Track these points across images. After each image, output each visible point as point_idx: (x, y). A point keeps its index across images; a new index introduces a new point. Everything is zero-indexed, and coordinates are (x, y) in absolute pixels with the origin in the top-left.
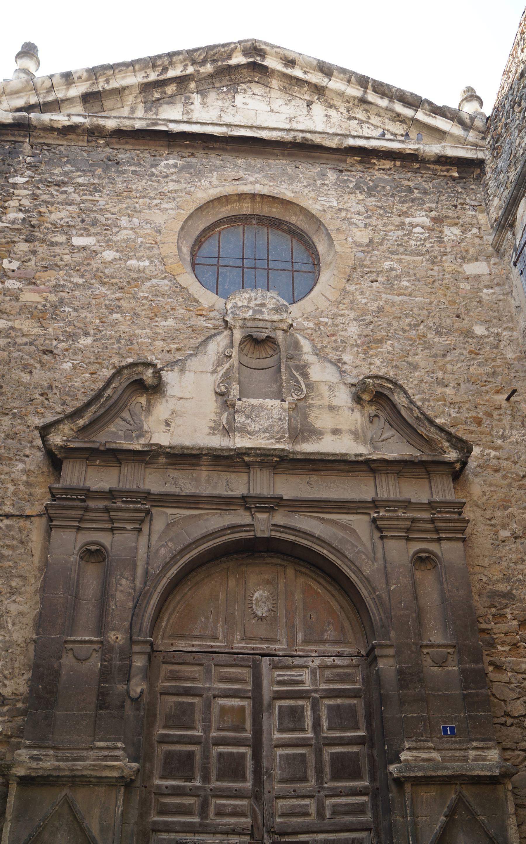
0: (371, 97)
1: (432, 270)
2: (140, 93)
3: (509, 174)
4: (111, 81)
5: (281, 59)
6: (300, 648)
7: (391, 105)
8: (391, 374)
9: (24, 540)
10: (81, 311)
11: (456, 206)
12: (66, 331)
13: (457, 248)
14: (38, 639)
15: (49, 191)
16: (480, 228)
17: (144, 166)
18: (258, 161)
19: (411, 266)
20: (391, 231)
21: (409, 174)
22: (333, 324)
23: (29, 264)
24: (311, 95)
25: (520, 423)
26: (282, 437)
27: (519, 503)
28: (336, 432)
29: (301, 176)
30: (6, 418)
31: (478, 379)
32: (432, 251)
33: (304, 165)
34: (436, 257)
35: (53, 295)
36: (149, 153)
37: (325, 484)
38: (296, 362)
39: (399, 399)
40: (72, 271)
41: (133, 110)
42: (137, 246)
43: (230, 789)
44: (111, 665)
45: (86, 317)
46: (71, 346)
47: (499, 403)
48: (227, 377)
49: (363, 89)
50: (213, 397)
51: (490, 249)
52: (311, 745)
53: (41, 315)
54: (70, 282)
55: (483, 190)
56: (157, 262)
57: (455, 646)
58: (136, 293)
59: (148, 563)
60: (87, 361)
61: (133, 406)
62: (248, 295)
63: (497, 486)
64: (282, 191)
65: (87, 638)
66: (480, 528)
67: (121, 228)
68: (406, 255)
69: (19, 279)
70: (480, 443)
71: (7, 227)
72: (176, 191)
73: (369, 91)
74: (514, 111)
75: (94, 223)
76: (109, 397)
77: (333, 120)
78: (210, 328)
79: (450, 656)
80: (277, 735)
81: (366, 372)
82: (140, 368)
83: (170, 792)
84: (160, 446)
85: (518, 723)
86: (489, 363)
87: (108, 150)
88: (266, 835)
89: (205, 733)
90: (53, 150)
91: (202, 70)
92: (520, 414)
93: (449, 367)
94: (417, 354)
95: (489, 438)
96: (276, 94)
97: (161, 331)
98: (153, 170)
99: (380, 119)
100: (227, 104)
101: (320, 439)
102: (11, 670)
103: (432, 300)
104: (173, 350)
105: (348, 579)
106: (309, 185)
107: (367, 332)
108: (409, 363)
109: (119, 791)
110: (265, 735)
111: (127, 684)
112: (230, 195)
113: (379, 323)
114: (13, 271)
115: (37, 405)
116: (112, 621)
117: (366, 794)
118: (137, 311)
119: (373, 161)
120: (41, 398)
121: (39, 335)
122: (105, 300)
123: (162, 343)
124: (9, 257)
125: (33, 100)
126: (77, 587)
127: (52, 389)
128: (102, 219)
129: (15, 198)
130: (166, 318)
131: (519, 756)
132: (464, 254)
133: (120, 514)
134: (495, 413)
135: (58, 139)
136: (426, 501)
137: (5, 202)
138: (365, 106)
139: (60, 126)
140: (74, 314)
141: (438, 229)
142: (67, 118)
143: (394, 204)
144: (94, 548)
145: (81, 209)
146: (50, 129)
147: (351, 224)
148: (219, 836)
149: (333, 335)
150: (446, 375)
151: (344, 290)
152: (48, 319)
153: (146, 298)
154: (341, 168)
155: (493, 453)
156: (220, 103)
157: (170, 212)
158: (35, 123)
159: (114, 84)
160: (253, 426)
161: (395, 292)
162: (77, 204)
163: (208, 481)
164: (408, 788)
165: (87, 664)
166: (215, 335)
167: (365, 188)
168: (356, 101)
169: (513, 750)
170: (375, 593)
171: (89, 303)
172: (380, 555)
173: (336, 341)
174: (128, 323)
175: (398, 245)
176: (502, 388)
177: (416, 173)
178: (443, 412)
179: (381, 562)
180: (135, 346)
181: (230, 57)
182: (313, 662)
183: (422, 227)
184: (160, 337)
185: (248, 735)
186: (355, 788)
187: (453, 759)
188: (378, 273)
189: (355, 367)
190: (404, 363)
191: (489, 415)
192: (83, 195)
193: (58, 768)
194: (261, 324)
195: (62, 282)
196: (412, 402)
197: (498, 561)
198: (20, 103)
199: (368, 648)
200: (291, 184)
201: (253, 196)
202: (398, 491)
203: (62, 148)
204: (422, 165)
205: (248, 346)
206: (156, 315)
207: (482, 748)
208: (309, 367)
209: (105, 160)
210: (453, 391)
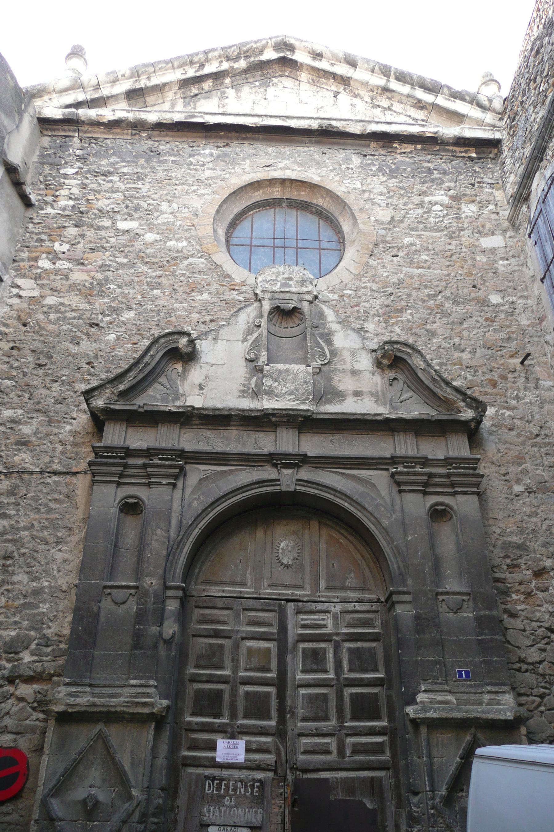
0: (394, 85)
1: (450, 244)
2: (179, 89)
3: (524, 150)
4: (152, 78)
5: (309, 52)
6: (323, 594)
7: (413, 92)
8: (410, 341)
9: (69, 495)
10: (124, 288)
11: (473, 185)
12: (111, 306)
13: (474, 224)
14: (79, 584)
15: (97, 180)
16: (496, 204)
17: (183, 156)
18: (287, 148)
19: (430, 241)
20: (411, 209)
21: (429, 157)
22: (356, 295)
23: (78, 246)
24: (337, 86)
25: (534, 385)
26: (307, 399)
27: (532, 459)
28: (357, 394)
29: (327, 161)
30: (56, 385)
31: (494, 345)
32: (451, 227)
33: (330, 151)
34: (454, 233)
35: (99, 274)
36: (188, 144)
37: (347, 442)
38: (320, 330)
39: (417, 362)
40: (117, 253)
41: (173, 105)
42: (176, 228)
43: (256, 726)
44: (146, 608)
45: (129, 293)
46: (115, 319)
47: (513, 367)
48: (256, 345)
49: (386, 78)
50: (244, 363)
51: (506, 224)
52: (333, 686)
53: (88, 292)
54: (116, 262)
55: (500, 169)
56: (194, 242)
57: (469, 594)
58: (175, 271)
59: (182, 515)
60: (129, 333)
61: (169, 372)
62: (277, 270)
63: (511, 444)
64: (310, 175)
65: (124, 584)
66: (495, 483)
67: (162, 213)
68: (426, 231)
69: (69, 260)
70: (495, 404)
71: (59, 214)
72: (212, 178)
73: (392, 79)
74: (529, 88)
75: (137, 208)
76: (147, 364)
77: (357, 109)
78: (242, 301)
79: (465, 603)
80: (300, 676)
81: (386, 339)
82: (176, 336)
83: (200, 728)
84: (194, 408)
85: (532, 669)
86: (504, 329)
87: (150, 142)
88: (288, 771)
89: (233, 673)
90: (100, 143)
91: (236, 65)
92: (534, 376)
93: (465, 333)
94: (435, 322)
95: (503, 399)
96: (305, 86)
97: (197, 305)
98: (191, 159)
99: (402, 105)
100: (260, 97)
101: (343, 401)
102: (55, 614)
103: (450, 272)
104: (208, 321)
105: (367, 530)
106: (335, 169)
107: (388, 302)
108: (427, 330)
109: (150, 727)
110: (289, 675)
111: (159, 626)
112: (262, 180)
113: (400, 294)
114: (64, 253)
115: (84, 372)
116: (147, 568)
117: (384, 734)
118: (175, 287)
119: (395, 145)
120: (87, 366)
121: (86, 310)
122: (146, 278)
123: (197, 315)
124: (60, 240)
125: (81, 97)
126: (117, 537)
127: (97, 358)
128: (144, 205)
129: (65, 187)
130: (201, 293)
131: (534, 701)
132: (481, 229)
133: (156, 470)
134: (510, 376)
135: (104, 133)
136: (443, 458)
137: (56, 191)
138: (388, 94)
139: (105, 121)
140: (118, 291)
141: (456, 206)
142: (112, 113)
143: (414, 184)
144: (132, 501)
145: (125, 196)
146: (96, 124)
147: (373, 203)
148: (244, 771)
149: (356, 306)
150: (463, 341)
151: (367, 264)
152: (95, 295)
153: (183, 275)
154: (364, 153)
155: (508, 413)
156: (253, 97)
157: (207, 197)
158: (83, 118)
159: (155, 81)
160: (279, 388)
161: (415, 265)
162: (121, 192)
163: (238, 440)
164: (424, 730)
165: (123, 607)
166: (246, 306)
167: (387, 171)
168: (380, 89)
169: (528, 696)
170: (393, 542)
171: (132, 281)
172: (398, 507)
173: (358, 311)
174: (167, 297)
175: (418, 222)
176: (516, 353)
177: (436, 155)
178: (459, 375)
179: (399, 514)
180: (173, 319)
181: (261, 52)
182: (335, 607)
183: (441, 205)
184: (196, 310)
185: (273, 675)
186: (374, 727)
187: (467, 702)
188: (399, 248)
189: (377, 335)
190: (423, 330)
191: (504, 378)
192: (127, 183)
193: (94, 705)
194: (287, 296)
195: (107, 263)
196: (429, 365)
197: (512, 514)
198: (70, 98)
199: (387, 594)
200: (318, 168)
201: (283, 182)
202: (415, 448)
203: (108, 142)
204: (442, 147)
205: (276, 316)
206: (192, 291)
207: (497, 693)
208: (333, 335)
209: (147, 151)
210: (469, 356)
